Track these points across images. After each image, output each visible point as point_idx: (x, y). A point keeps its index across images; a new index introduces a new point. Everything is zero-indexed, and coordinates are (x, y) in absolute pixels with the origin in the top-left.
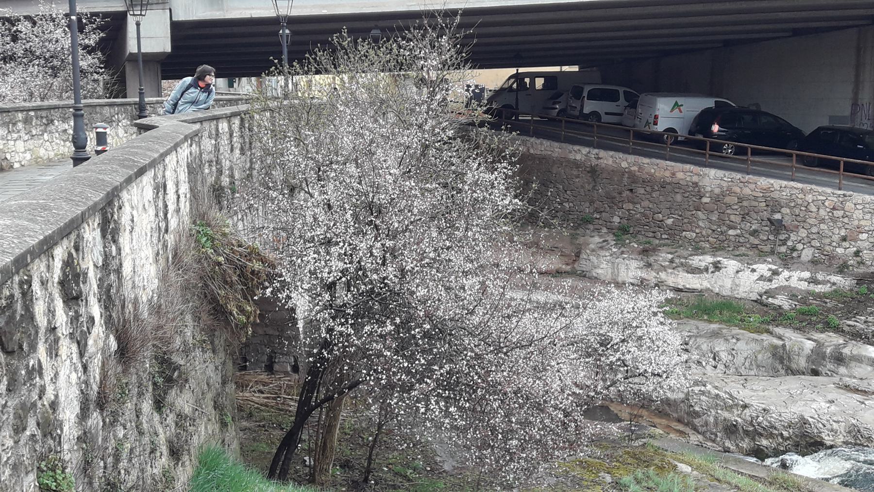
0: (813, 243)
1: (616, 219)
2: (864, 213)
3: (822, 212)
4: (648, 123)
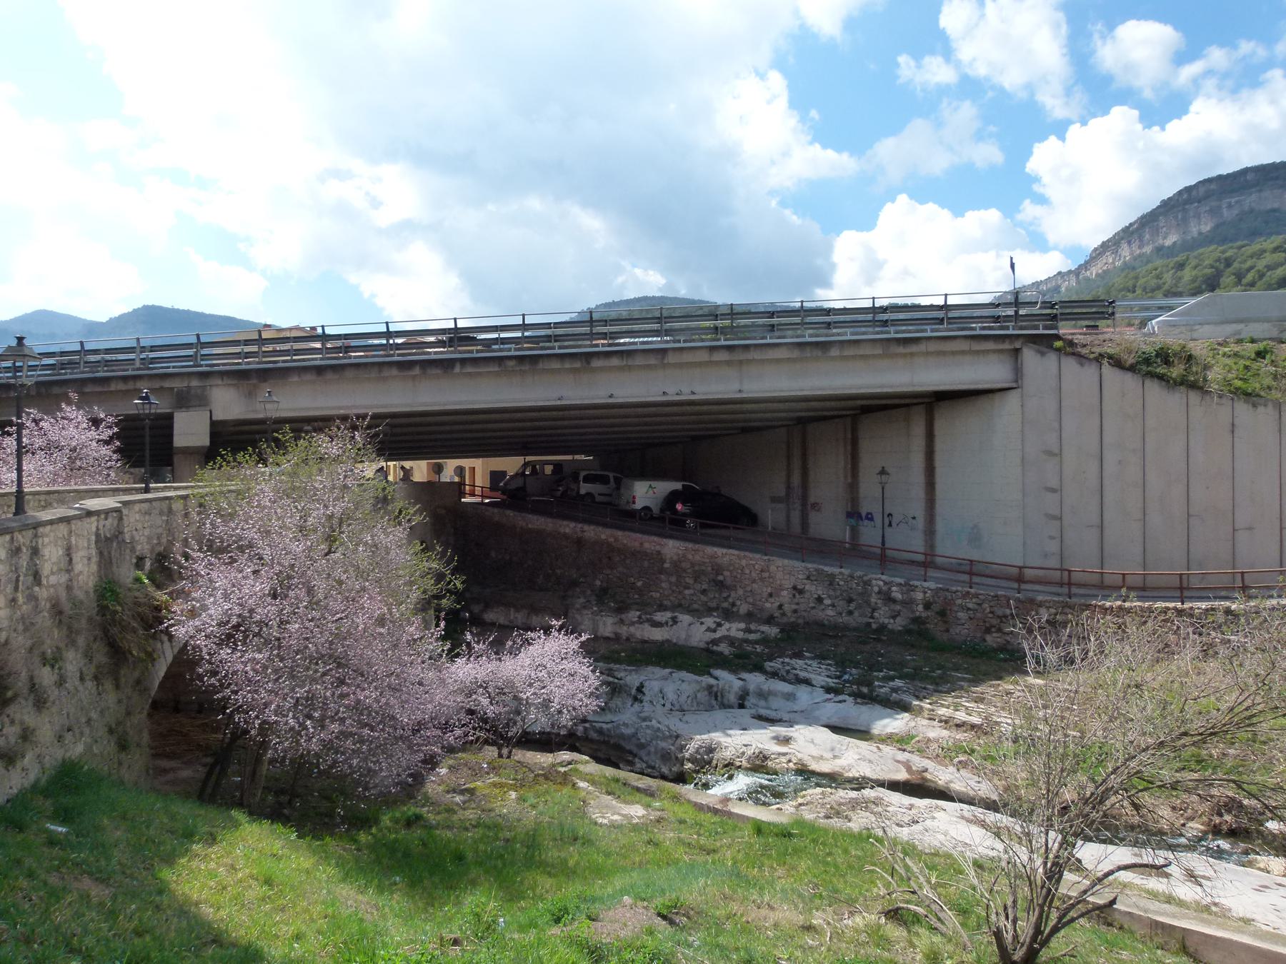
1: (598, 583)
3: (754, 575)
4: (628, 502)
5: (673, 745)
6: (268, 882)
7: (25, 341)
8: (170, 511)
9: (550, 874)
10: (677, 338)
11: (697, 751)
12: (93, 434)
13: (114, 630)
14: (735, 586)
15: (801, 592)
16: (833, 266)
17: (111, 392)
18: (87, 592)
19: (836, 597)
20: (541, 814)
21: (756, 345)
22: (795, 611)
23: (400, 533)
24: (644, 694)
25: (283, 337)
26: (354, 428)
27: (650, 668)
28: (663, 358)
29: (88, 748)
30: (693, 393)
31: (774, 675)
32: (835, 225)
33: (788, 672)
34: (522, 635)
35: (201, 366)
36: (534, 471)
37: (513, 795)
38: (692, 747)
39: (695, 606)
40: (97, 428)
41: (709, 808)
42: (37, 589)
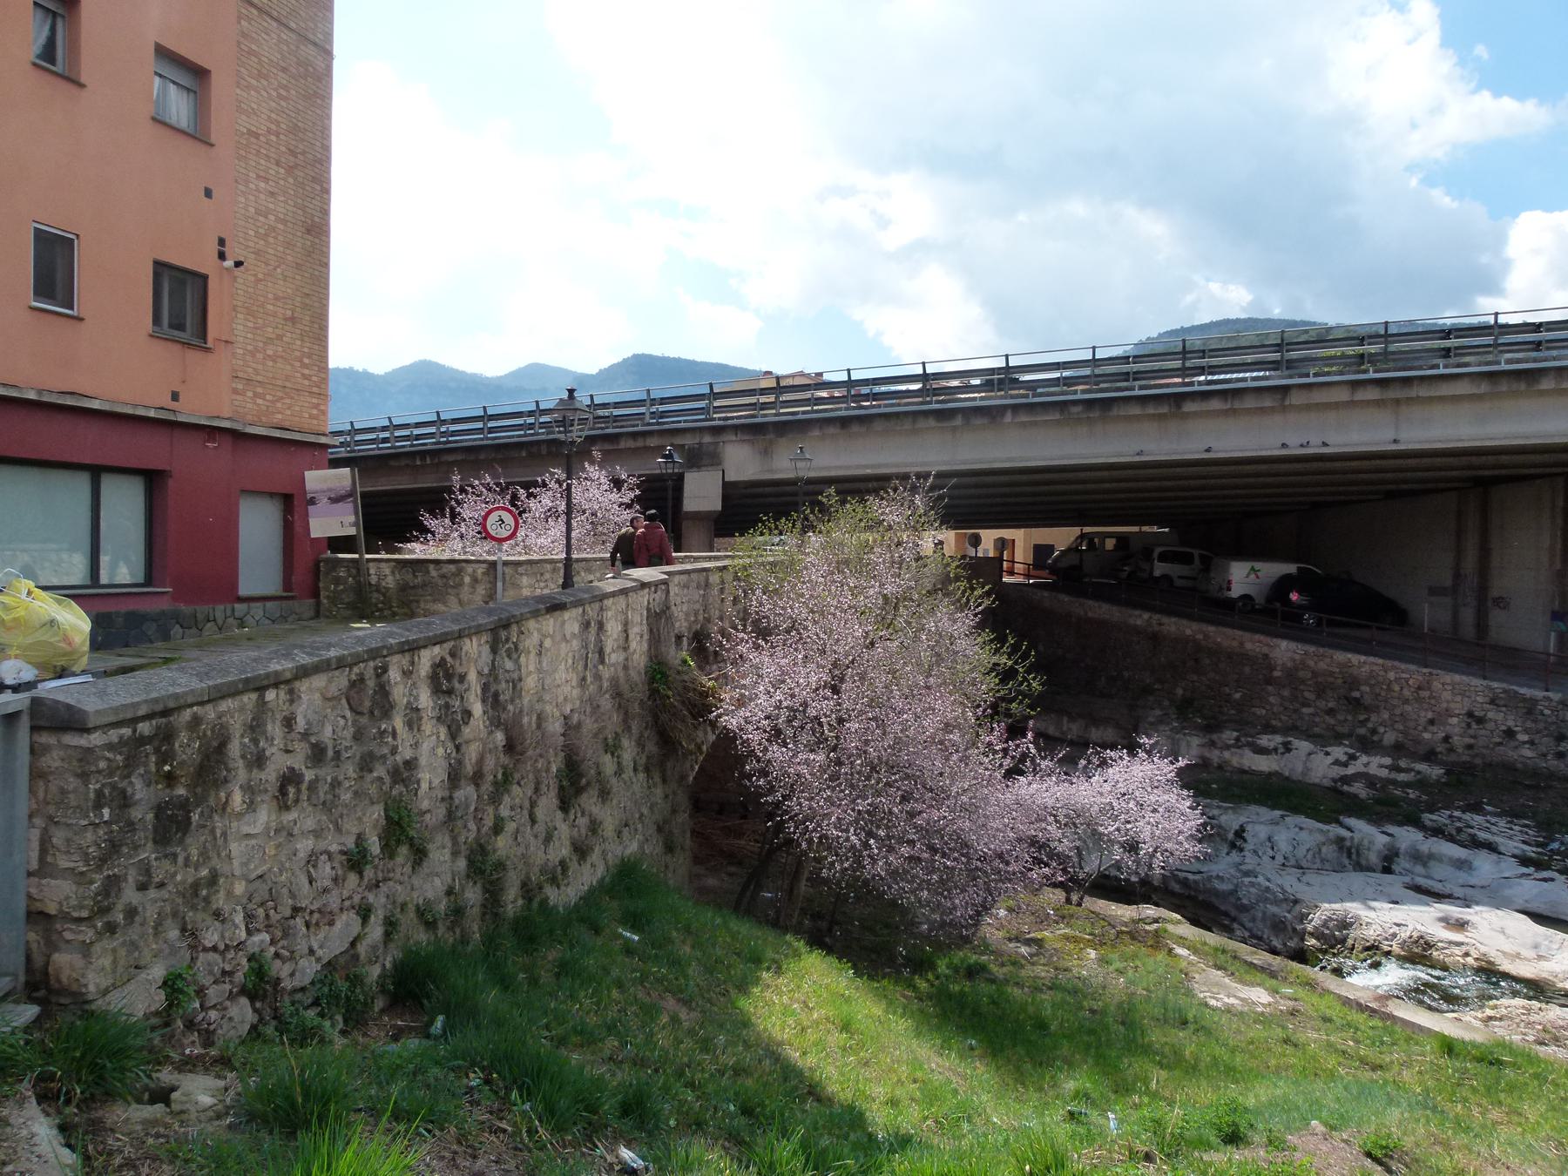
0: (1396, 726)
1: (1180, 691)
2: (1454, 694)
3: (1406, 693)
4: (1221, 589)
5: (1289, 912)
6: (846, 1027)
7: (576, 394)
8: (707, 585)
9: (1161, 1065)
10: (1304, 371)
11: (1325, 924)
12: (614, 496)
13: (664, 717)
14: (1378, 707)
15: (1480, 721)
16: (1507, 264)
17: (1412, 399)
18: (639, 673)
19: (1538, 732)
20: (1132, 982)
21: (1422, 378)
22: (1470, 747)
23: (967, 621)
24: (1245, 841)
25: (780, 387)
26: (914, 490)
27: (1253, 808)
28: (1283, 399)
29: (641, 847)
30: (1325, 444)
31: (1437, 832)
32: (1509, 205)
33: (1459, 830)
34: (1099, 753)
35: (714, 419)
36: (1091, 544)
37: (1092, 954)
38: (1316, 919)
39: (1317, 730)
40: (619, 490)
41: (1359, 1005)
42: (601, 667)
